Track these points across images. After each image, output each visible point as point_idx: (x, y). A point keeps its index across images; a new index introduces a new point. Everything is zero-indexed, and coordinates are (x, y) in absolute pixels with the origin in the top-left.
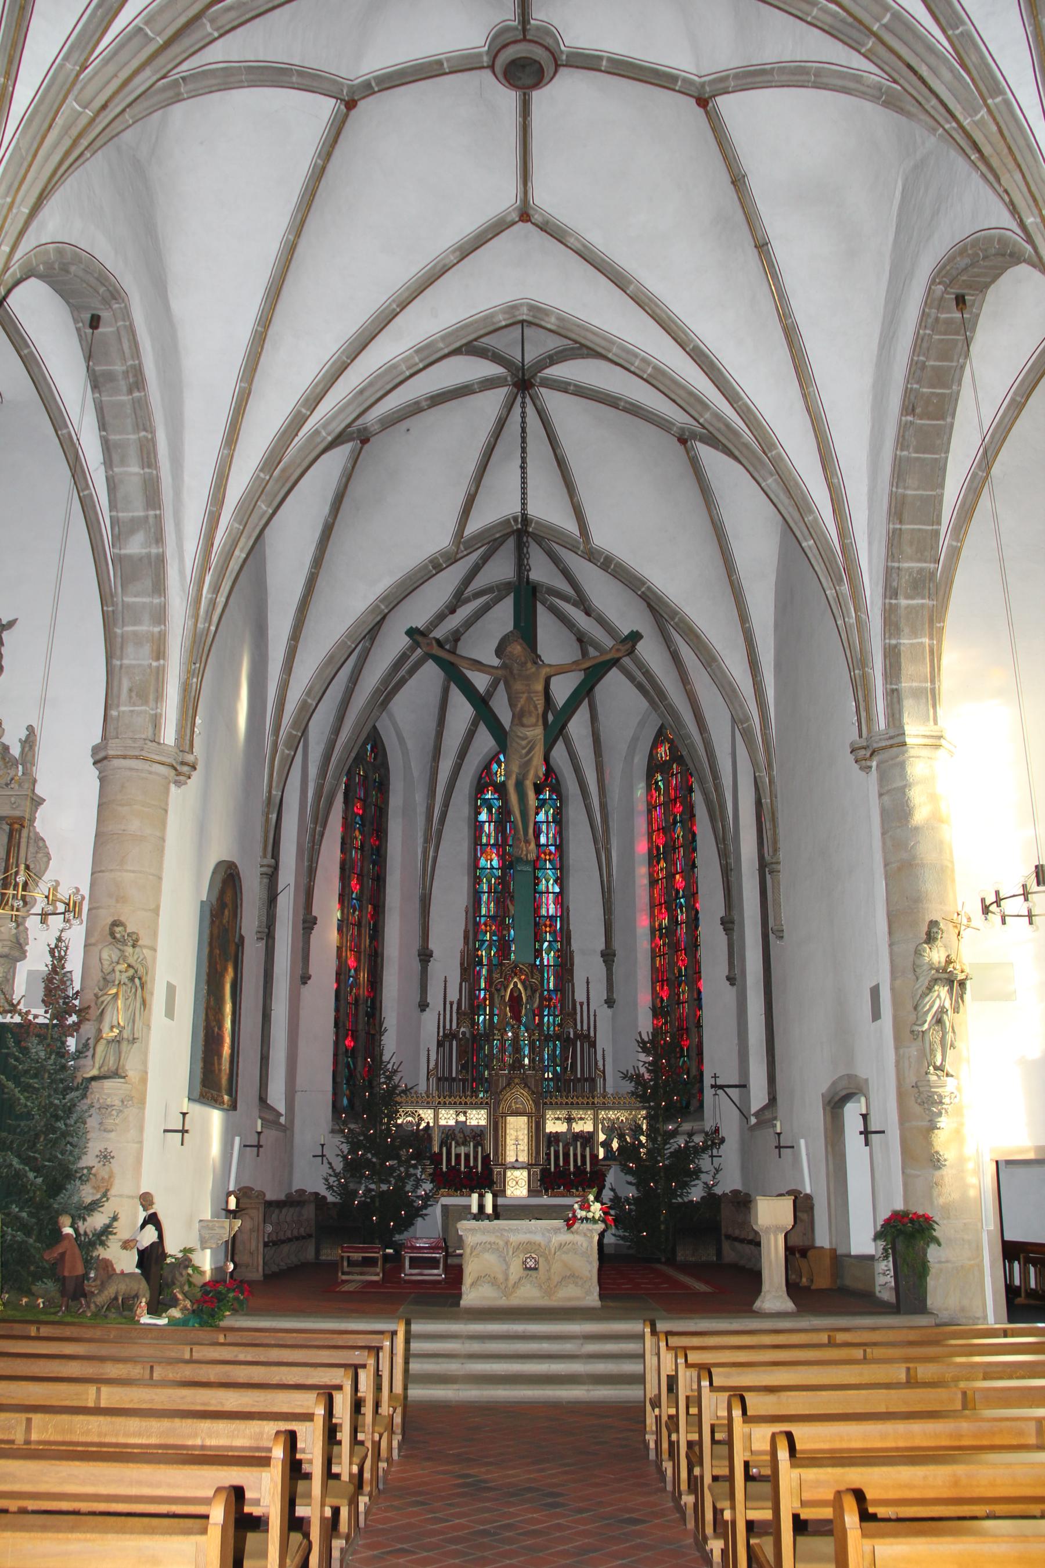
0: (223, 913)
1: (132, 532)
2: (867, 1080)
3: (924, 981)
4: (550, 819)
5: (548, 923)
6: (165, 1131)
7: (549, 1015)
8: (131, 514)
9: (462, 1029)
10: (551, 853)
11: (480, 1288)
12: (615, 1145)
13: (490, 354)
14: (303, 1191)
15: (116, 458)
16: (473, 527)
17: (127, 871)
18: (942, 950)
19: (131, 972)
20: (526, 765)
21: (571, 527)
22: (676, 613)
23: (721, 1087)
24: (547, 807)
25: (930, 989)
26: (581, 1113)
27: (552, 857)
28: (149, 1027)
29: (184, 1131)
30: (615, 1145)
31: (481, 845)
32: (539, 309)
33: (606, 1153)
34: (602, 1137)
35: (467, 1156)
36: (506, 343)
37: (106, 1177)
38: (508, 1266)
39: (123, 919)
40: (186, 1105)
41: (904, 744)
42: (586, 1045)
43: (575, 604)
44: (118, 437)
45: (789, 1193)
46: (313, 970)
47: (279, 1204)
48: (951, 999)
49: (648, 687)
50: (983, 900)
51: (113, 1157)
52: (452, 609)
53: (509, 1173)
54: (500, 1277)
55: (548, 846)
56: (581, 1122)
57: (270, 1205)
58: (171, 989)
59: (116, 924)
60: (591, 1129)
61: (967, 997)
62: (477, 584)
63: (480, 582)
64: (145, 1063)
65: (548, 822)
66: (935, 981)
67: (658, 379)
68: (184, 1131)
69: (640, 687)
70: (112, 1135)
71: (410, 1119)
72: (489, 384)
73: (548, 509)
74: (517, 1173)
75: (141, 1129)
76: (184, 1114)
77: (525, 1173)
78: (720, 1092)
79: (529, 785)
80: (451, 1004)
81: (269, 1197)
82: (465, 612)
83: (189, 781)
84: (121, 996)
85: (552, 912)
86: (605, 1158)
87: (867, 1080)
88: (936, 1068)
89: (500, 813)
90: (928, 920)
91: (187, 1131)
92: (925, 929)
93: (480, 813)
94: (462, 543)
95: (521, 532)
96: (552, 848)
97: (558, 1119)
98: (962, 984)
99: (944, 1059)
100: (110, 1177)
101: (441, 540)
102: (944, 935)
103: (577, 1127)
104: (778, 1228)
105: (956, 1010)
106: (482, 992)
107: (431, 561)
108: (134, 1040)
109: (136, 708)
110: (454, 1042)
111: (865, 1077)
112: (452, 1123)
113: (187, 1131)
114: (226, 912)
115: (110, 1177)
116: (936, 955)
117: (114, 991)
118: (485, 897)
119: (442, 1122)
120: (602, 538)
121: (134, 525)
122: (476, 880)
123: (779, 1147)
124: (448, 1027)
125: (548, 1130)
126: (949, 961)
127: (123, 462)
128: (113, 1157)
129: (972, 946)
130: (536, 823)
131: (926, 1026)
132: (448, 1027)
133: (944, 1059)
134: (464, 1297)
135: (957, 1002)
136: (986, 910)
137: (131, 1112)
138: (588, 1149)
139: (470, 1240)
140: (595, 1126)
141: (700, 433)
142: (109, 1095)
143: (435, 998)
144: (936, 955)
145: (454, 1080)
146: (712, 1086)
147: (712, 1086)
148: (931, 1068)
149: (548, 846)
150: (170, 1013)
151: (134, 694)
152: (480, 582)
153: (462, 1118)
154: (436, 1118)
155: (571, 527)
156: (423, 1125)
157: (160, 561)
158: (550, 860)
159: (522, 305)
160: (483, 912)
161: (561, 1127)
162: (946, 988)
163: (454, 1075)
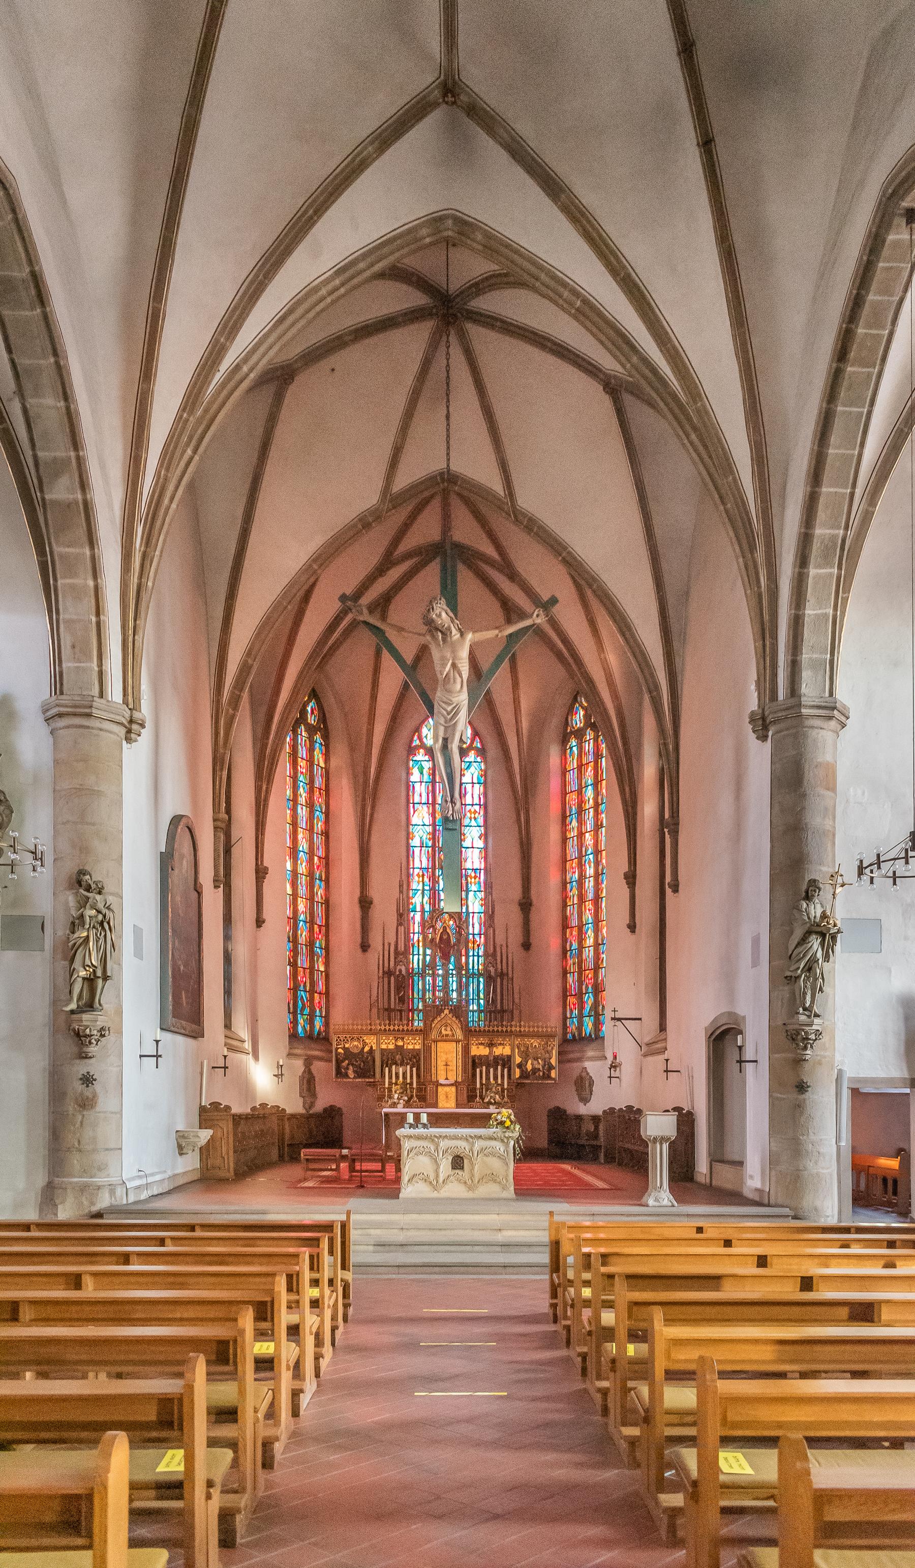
0: (182, 864)
1: (57, 475)
2: (744, 1018)
3: (798, 933)
4: (475, 781)
5: (473, 875)
6: (141, 1056)
7: (474, 956)
8: (53, 454)
9: (398, 967)
10: (475, 812)
11: (416, 1185)
12: (529, 1067)
13: (414, 279)
14: (263, 1105)
15: (28, 386)
16: (401, 482)
17: (518, 795)
18: (818, 906)
19: (100, 917)
20: (450, 727)
21: (498, 488)
22: (594, 579)
23: (619, 1019)
24: (472, 769)
25: (804, 940)
26: (500, 1040)
27: (477, 815)
28: (120, 965)
29: (158, 1056)
30: (529, 1067)
31: (414, 803)
32: (466, 223)
33: (522, 1072)
34: (518, 1060)
35: (404, 1074)
36: (426, 264)
37: (91, 1096)
38: (438, 1166)
39: (86, 868)
40: (159, 1034)
41: (800, 716)
42: (505, 982)
43: (500, 570)
44: (28, 362)
45: (675, 1109)
46: (266, 915)
47: (246, 1118)
48: (823, 950)
49: (566, 654)
50: (861, 861)
51: (95, 1080)
52: (380, 571)
53: (440, 1089)
54: (432, 1177)
55: (473, 805)
56: (500, 1047)
57: (238, 1119)
58: (137, 931)
59: (82, 872)
60: (509, 1053)
61: (838, 948)
62: (402, 548)
63: (411, 542)
64: (119, 996)
65: (473, 783)
66: (809, 933)
67: (587, 312)
68: (158, 1056)
69: (559, 656)
70: (92, 1061)
71: (356, 1043)
72: (413, 316)
73: (476, 465)
74: (447, 1089)
75: (120, 1055)
76: (157, 1042)
77: (454, 1089)
78: (618, 1023)
79: (454, 747)
80: (389, 944)
81: (235, 1110)
82: (395, 574)
83: (139, 738)
84: (91, 939)
85: (476, 866)
86: (520, 1077)
87: (744, 1018)
88: (805, 1009)
89: (429, 774)
90: (807, 880)
91: (160, 1056)
92: (804, 887)
93: (412, 774)
94: (391, 500)
95: (446, 487)
96: (477, 808)
97: (482, 1044)
98: (834, 938)
99: (813, 1001)
100: (94, 1097)
101: (370, 498)
102: (821, 893)
103: (498, 1051)
104: (663, 1139)
105: (827, 958)
106: (416, 935)
107: (360, 520)
108: (106, 978)
109: (82, 665)
110: (392, 979)
111: (743, 1014)
112: (391, 1047)
113: (160, 1056)
114: (185, 863)
115: (94, 1097)
116: (815, 910)
117: (85, 934)
118: (417, 851)
119: (384, 1046)
120: (526, 501)
121: (59, 467)
122: (409, 836)
123: (667, 1071)
124: (386, 965)
125: (473, 1054)
126: (824, 916)
127: (37, 394)
128: (95, 1080)
129: (843, 904)
130: (461, 784)
131: (799, 971)
132: (386, 965)
133: (813, 1001)
134: (403, 1190)
135: (827, 952)
136: (861, 871)
137: (110, 1039)
138: (506, 1070)
139: (406, 1145)
140: (513, 1050)
141: (627, 382)
142: (87, 1027)
143: (376, 940)
144: (815, 910)
145: (394, 1010)
146: (612, 1019)
147: (612, 1019)
148: (801, 1009)
149: (473, 805)
150: (138, 954)
151: (77, 650)
152: (411, 542)
153: (400, 1043)
154: (378, 1044)
155: (498, 488)
156: (367, 1049)
157: (88, 507)
158: (475, 818)
159: (446, 217)
160: (417, 864)
161: (484, 1051)
162: (819, 940)
163: (392, 1007)
